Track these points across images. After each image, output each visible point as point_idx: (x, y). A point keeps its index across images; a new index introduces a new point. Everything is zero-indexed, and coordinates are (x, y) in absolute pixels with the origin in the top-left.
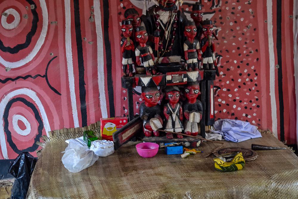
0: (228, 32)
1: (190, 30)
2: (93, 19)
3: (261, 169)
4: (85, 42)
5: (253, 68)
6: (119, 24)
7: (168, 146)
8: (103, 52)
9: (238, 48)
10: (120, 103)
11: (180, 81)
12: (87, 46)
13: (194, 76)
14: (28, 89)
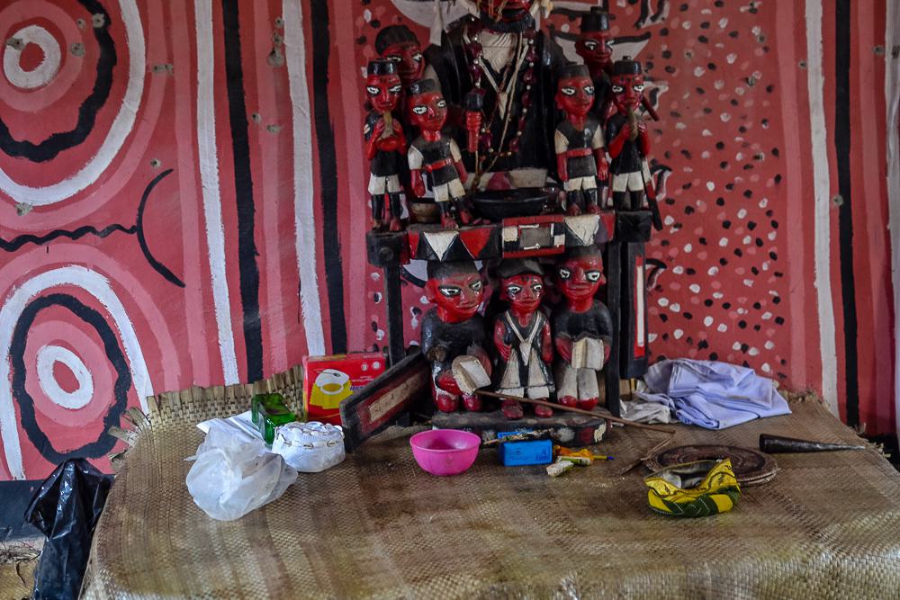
0: (689, 97)
1: (573, 91)
2: (282, 56)
3: (789, 510)
4: (258, 126)
5: (763, 204)
6: (359, 72)
7: (508, 439)
8: (310, 156)
9: (720, 146)
10: (364, 310)
11: (544, 244)
12: (261, 140)
13: (585, 228)
14: (85, 269)
